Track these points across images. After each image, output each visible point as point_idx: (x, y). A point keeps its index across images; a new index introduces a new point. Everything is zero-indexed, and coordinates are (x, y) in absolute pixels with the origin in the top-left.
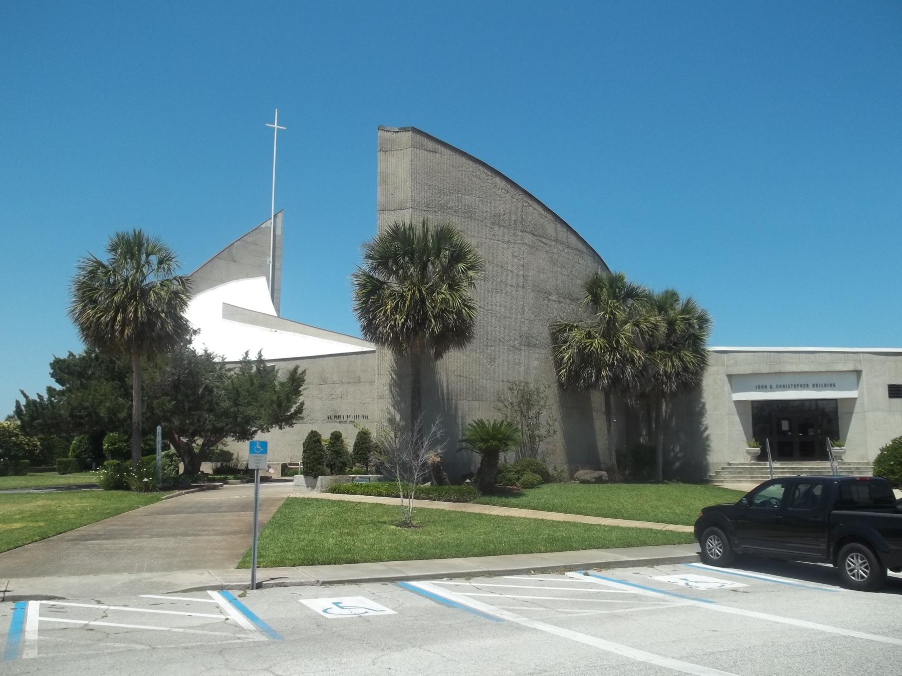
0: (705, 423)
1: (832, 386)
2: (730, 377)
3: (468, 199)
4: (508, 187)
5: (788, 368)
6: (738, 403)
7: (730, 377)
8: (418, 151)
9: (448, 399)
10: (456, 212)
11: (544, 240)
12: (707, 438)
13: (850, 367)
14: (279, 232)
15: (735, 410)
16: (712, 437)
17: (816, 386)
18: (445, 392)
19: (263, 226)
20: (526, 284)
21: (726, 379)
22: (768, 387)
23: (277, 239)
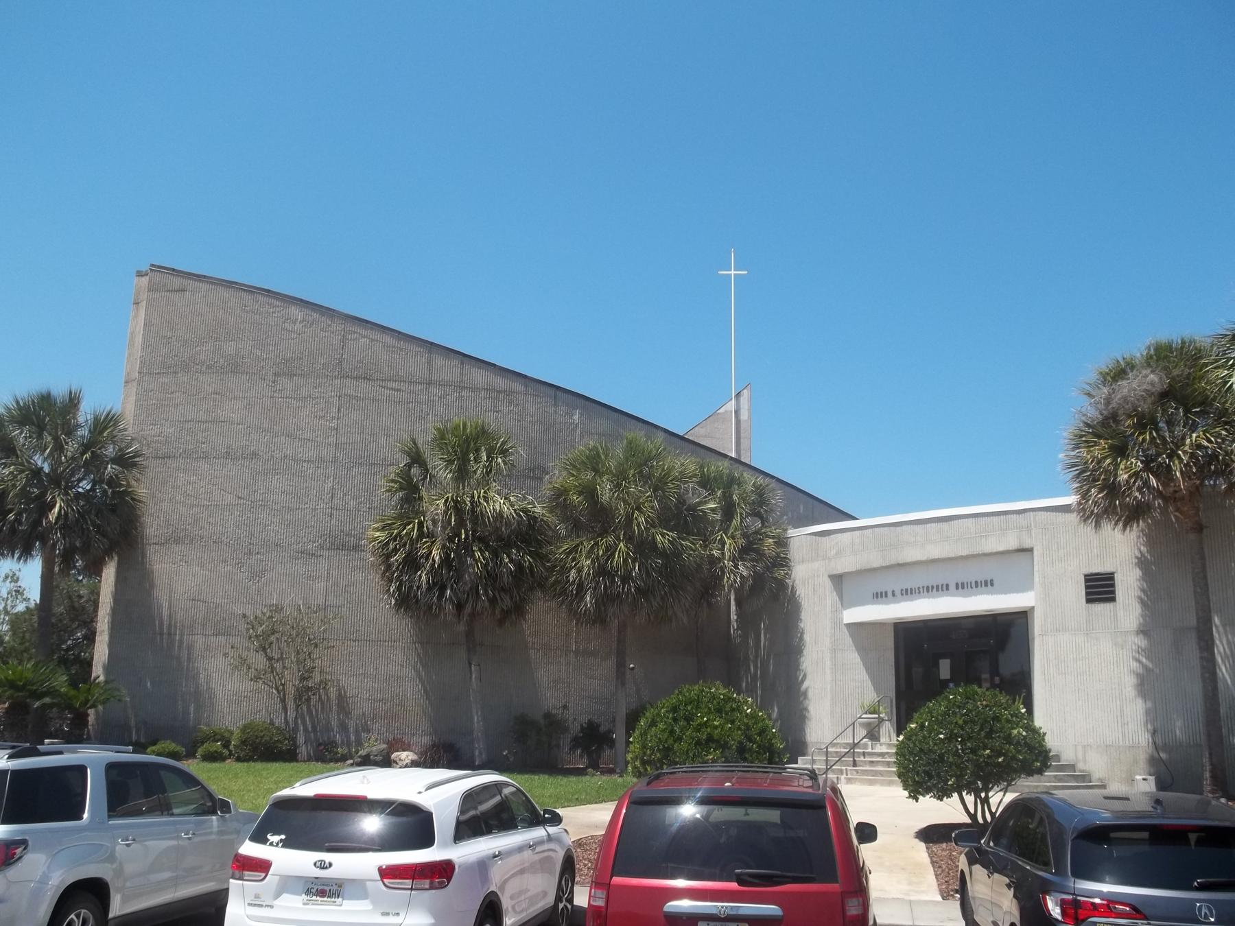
0: (803, 667)
1: (987, 584)
2: (838, 580)
3: (231, 347)
4: (316, 315)
5: (912, 554)
6: (857, 629)
7: (838, 580)
8: (157, 295)
9: (169, 634)
10: (209, 367)
11: (395, 385)
12: (805, 694)
13: (1011, 542)
14: (744, 416)
15: (849, 640)
16: (810, 694)
17: (962, 587)
18: (166, 623)
19: (721, 411)
20: (341, 456)
21: (828, 583)
22: (890, 594)
23: (743, 426)
